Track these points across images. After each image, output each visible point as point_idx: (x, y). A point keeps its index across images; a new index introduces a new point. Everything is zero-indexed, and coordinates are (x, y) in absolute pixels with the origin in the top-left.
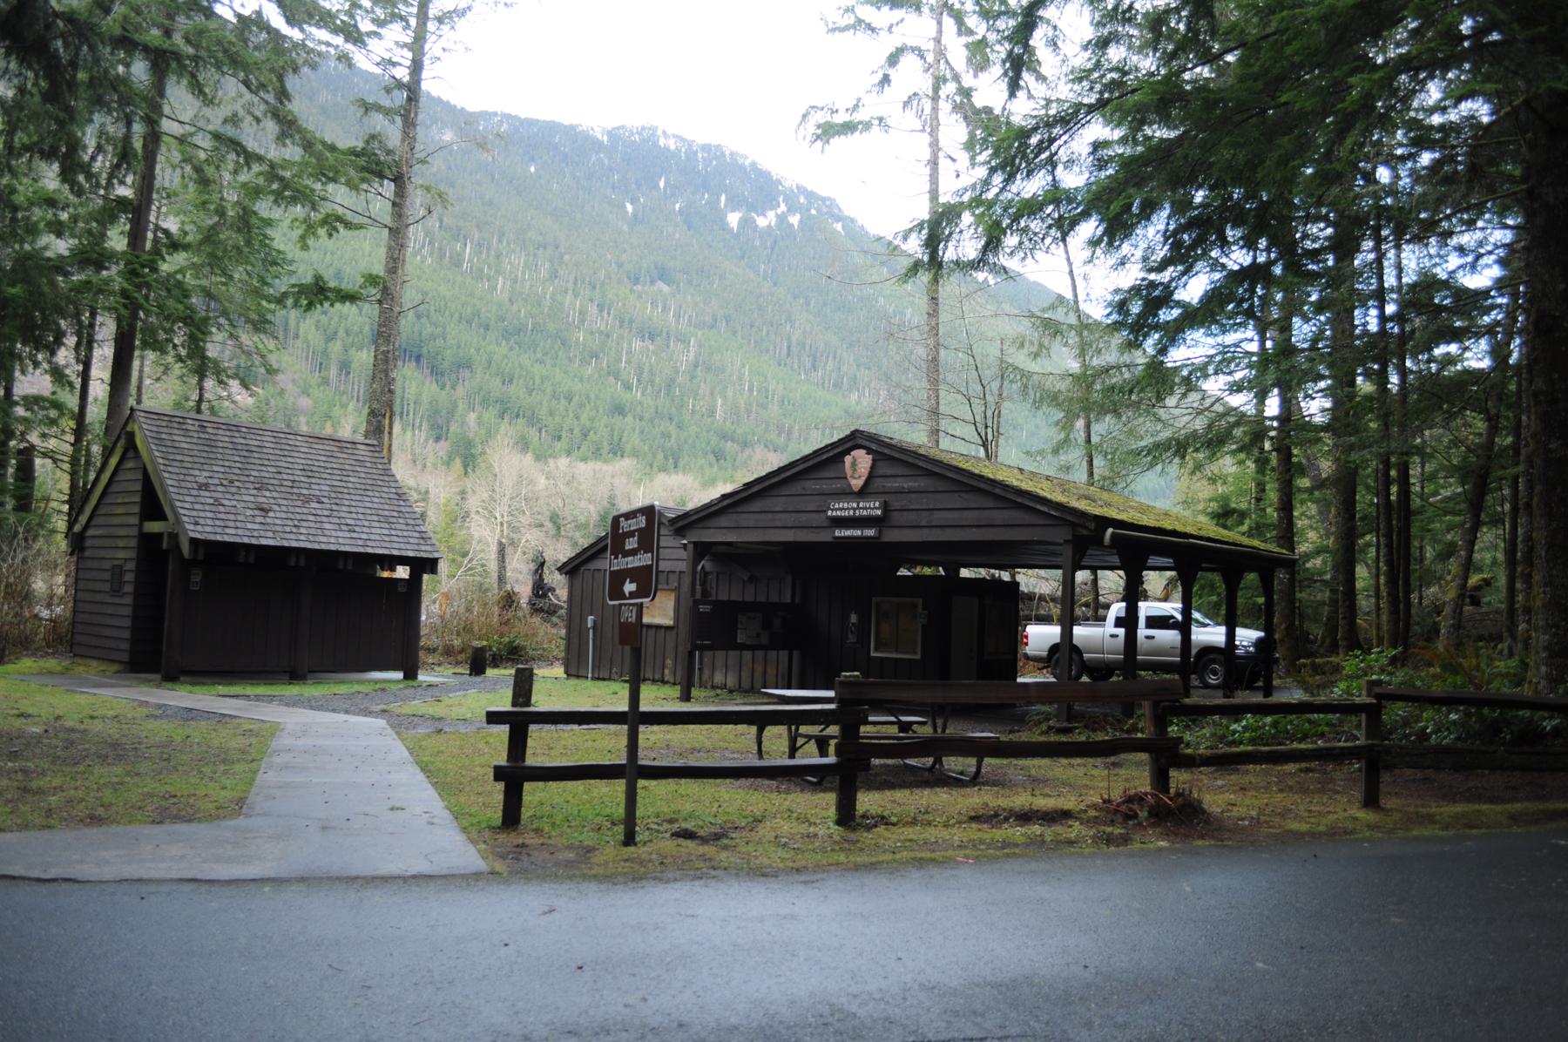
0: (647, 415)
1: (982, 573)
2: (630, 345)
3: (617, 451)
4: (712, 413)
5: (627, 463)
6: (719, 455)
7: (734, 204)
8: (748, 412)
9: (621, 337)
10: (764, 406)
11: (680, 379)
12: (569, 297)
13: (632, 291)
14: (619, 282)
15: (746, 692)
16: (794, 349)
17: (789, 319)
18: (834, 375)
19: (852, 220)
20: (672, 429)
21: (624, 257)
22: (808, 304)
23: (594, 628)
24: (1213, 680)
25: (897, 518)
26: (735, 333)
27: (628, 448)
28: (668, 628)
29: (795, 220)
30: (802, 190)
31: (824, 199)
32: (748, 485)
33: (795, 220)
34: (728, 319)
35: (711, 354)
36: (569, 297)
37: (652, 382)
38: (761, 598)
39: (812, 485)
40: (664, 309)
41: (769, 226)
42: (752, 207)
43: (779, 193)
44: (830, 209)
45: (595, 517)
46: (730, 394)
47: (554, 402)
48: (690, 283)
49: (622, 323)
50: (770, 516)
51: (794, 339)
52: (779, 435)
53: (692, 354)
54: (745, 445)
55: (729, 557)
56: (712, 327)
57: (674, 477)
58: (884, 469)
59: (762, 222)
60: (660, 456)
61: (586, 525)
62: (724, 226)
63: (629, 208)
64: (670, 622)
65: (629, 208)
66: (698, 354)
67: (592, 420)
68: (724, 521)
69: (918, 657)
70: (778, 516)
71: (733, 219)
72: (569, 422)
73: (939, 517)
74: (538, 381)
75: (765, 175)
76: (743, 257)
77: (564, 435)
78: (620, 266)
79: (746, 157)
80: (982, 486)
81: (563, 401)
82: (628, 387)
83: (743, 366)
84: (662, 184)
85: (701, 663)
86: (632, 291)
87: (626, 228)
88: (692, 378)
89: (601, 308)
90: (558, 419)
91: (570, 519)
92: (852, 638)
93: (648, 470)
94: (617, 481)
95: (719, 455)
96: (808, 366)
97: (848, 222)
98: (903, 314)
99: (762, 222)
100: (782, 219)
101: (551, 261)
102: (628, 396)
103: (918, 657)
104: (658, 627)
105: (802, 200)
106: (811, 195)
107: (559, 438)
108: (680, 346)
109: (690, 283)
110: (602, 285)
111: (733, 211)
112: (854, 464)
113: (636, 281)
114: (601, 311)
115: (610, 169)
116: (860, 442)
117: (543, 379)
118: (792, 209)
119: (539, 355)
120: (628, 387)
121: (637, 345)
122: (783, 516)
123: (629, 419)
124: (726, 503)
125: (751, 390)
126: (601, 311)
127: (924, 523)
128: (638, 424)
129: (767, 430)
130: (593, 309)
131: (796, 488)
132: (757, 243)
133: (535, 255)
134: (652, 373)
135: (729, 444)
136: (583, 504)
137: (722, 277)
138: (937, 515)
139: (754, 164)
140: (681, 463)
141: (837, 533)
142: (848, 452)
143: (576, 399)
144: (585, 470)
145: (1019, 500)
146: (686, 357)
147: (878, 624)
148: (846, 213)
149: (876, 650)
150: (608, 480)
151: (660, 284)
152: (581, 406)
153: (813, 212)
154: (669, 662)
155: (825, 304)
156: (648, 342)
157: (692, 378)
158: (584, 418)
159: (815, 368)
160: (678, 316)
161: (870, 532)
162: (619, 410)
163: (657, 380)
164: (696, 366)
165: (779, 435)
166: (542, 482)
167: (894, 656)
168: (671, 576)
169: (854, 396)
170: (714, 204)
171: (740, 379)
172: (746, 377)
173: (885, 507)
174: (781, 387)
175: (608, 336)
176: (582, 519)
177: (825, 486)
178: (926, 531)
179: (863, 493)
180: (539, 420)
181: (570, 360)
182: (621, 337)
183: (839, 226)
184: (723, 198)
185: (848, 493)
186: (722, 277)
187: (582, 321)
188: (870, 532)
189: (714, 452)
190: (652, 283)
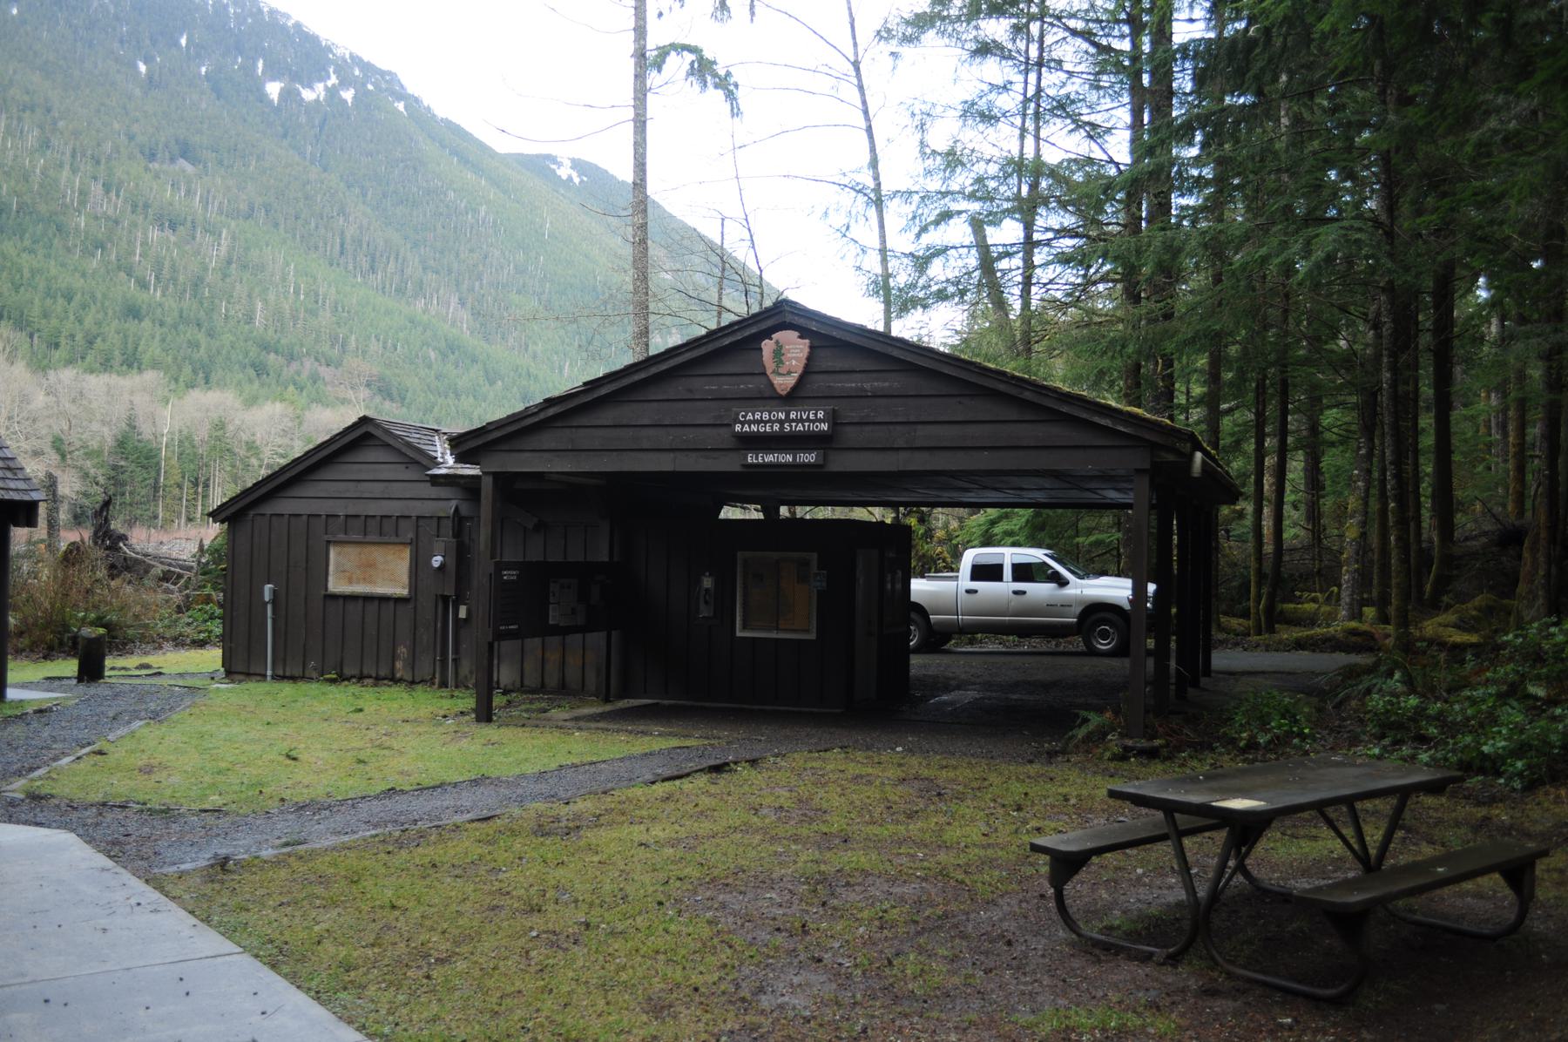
0: (169, 320)
1: (859, 514)
2: (145, 234)
3: (132, 362)
4: (250, 319)
5: (150, 376)
6: (260, 369)
7: (274, 72)
8: (295, 318)
9: (134, 225)
10: (313, 313)
11: (209, 278)
12: (66, 173)
13: (147, 169)
14: (131, 157)
15: (533, 692)
16: (348, 246)
17: (342, 212)
18: (397, 278)
19: (417, 100)
20: (201, 337)
21: (135, 128)
22: (364, 195)
23: (274, 601)
24: (1103, 645)
25: (851, 435)
26: (276, 225)
27: (146, 358)
28: (399, 600)
29: (348, 95)
30: (357, 60)
31: (383, 73)
32: (592, 385)
33: (348, 95)
34: (268, 208)
35: (247, 249)
36: (66, 173)
37: (174, 280)
38: (576, 556)
39: (703, 385)
40: (188, 192)
41: (317, 101)
42: (295, 77)
43: (330, 62)
44: (389, 84)
45: (110, 442)
46: (272, 297)
47: (49, 301)
48: (220, 163)
49: (135, 206)
50: (630, 432)
51: (348, 235)
52: (333, 346)
53: (224, 249)
54: (291, 358)
55: (519, 496)
56: (248, 217)
57: (210, 394)
58: (828, 361)
59: (308, 95)
60: (187, 370)
61: (99, 453)
62: (263, 98)
63: (143, 68)
64: (405, 592)
65: (143, 68)
66: (231, 249)
67: (98, 324)
68: (548, 439)
69: (813, 636)
70: (645, 432)
71: (273, 89)
72: (69, 326)
73: (923, 435)
74: (26, 274)
75: (314, 39)
76: (285, 136)
77: (63, 341)
78: (131, 138)
79: (288, 17)
80: (1002, 387)
81: (60, 301)
82: (143, 285)
83: (288, 265)
84: (183, 41)
85: (456, 651)
86: (147, 169)
87: (138, 92)
88: (225, 276)
89: (107, 188)
90: (54, 322)
91: (78, 444)
92: (705, 611)
93: (173, 386)
94: (137, 399)
95: (260, 369)
96: (366, 266)
97: (413, 102)
98: (475, 211)
99: (308, 95)
100: (332, 93)
101: (41, 127)
102: (145, 296)
103: (813, 636)
104: (383, 599)
105: (357, 72)
106: (367, 67)
107: (57, 346)
108: (208, 238)
109: (220, 163)
110: (109, 158)
111: (273, 79)
112: (778, 353)
113: (152, 157)
114: (107, 192)
115: (117, 18)
116: (789, 318)
117: (33, 272)
118: (344, 82)
119: (27, 243)
120: (143, 285)
121: (154, 234)
122: (651, 432)
123: (146, 324)
124: (551, 412)
125: (297, 292)
126: (107, 192)
127: (901, 443)
128: (159, 331)
129: (317, 341)
130: (96, 189)
131: (677, 388)
132: (303, 119)
133: (20, 119)
134: (174, 269)
135: (272, 356)
136: (95, 426)
137: (260, 158)
138: (922, 431)
139: (298, 26)
140: (214, 378)
141: (751, 459)
142: (767, 334)
143: (78, 297)
144: (96, 384)
145: (1065, 409)
146: (216, 252)
147: (745, 587)
148: (410, 91)
149: (745, 627)
150: (126, 397)
151: (182, 162)
152: (84, 306)
153: (370, 87)
154: (402, 650)
155: (385, 196)
156: (168, 232)
157: (225, 276)
158: (89, 321)
159: (373, 269)
160: (205, 203)
161: (809, 458)
162: (133, 312)
163: (181, 278)
164: (229, 262)
165: (333, 346)
166: (40, 399)
167: (774, 635)
168: (402, 523)
169: (420, 304)
170: (248, 70)
171: (284, 279)
172: (291, 277)
173: (833, 418)
174: (333, 290)
175: (117, 222)
176: (94, 444)
177: (727, 386)
178: (903, 455)
179: (793, 398)
180: (29, 324)
181: (69, 250)
182: (134, 225)
183: (401, 106)
184: (260, 64)
185: (771, 398)
186: (260, 158)
187: (83, 203)
188: (809, 458)
189: (253, 365)
190: (172, 160)
